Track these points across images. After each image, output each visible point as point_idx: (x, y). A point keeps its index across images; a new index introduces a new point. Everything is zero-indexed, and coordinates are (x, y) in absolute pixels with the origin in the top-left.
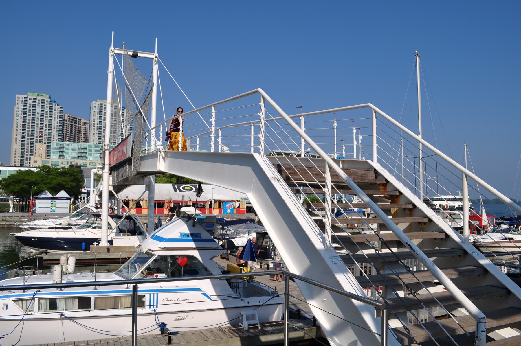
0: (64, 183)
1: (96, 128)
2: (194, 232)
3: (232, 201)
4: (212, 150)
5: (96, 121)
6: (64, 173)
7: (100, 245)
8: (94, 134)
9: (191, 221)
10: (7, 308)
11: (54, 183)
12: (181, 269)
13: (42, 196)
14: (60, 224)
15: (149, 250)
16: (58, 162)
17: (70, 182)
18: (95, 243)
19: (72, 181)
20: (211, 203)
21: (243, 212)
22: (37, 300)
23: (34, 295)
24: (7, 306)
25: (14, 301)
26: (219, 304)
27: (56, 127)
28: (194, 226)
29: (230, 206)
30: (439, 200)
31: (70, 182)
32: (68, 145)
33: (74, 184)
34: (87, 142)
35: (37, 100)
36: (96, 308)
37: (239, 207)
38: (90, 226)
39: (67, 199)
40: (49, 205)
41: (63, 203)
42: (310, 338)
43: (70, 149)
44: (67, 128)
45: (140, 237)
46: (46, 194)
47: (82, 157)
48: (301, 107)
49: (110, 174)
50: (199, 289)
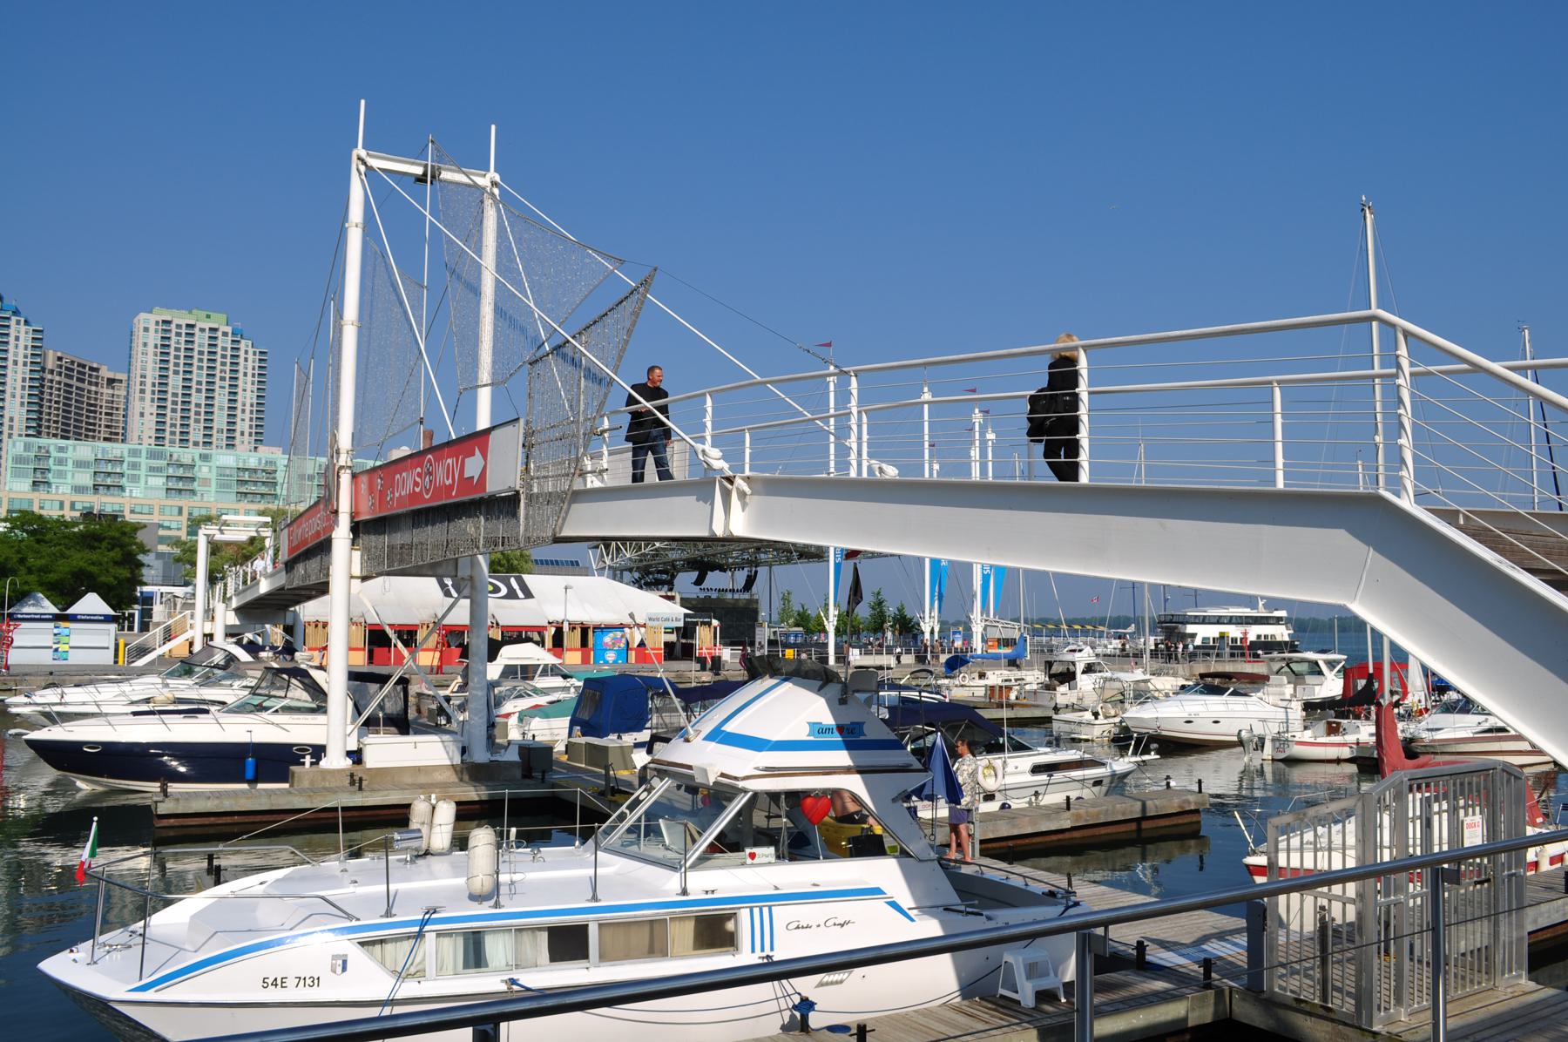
0: (93, 569)
1: (148, 396)
2: (846, 721)
3: (621, 627)
4: (853, 474)
5: (149, 374)
6: (90, 540)
7: (323, 764)
8: (142, 415)
9: (834, 689)
10: (344, 969)
11: (63, 569)
12: (802, 827)
13: (25, 610)
14: (147, 701)
15: (723, 775)
16: (31, 502)
17: (98, 563)
18: (308, 760)
19: (116, 563)
20: (559, 631)
22: (430, 938)
23: (424, 923)
24: (345, 962)
25: (362, 944)
27: (18, 392)
28: (843, 701)
29: (616, 641)
30: (1204, 621)
31: (98, 563)
32: (61, 449)
33: (124, 573)
34: (116, 441)
35: (173, 326)
36: (604, 957)
37: (642, 644)
38: (261, 708)
40: (48, 640)
41: (90, 636)
43: (70, 463)
44: (53, 395)
45: (446, 737)
46: (38, 603)
47: (108, 487)
48: (829, 345)
50: (877, 891)
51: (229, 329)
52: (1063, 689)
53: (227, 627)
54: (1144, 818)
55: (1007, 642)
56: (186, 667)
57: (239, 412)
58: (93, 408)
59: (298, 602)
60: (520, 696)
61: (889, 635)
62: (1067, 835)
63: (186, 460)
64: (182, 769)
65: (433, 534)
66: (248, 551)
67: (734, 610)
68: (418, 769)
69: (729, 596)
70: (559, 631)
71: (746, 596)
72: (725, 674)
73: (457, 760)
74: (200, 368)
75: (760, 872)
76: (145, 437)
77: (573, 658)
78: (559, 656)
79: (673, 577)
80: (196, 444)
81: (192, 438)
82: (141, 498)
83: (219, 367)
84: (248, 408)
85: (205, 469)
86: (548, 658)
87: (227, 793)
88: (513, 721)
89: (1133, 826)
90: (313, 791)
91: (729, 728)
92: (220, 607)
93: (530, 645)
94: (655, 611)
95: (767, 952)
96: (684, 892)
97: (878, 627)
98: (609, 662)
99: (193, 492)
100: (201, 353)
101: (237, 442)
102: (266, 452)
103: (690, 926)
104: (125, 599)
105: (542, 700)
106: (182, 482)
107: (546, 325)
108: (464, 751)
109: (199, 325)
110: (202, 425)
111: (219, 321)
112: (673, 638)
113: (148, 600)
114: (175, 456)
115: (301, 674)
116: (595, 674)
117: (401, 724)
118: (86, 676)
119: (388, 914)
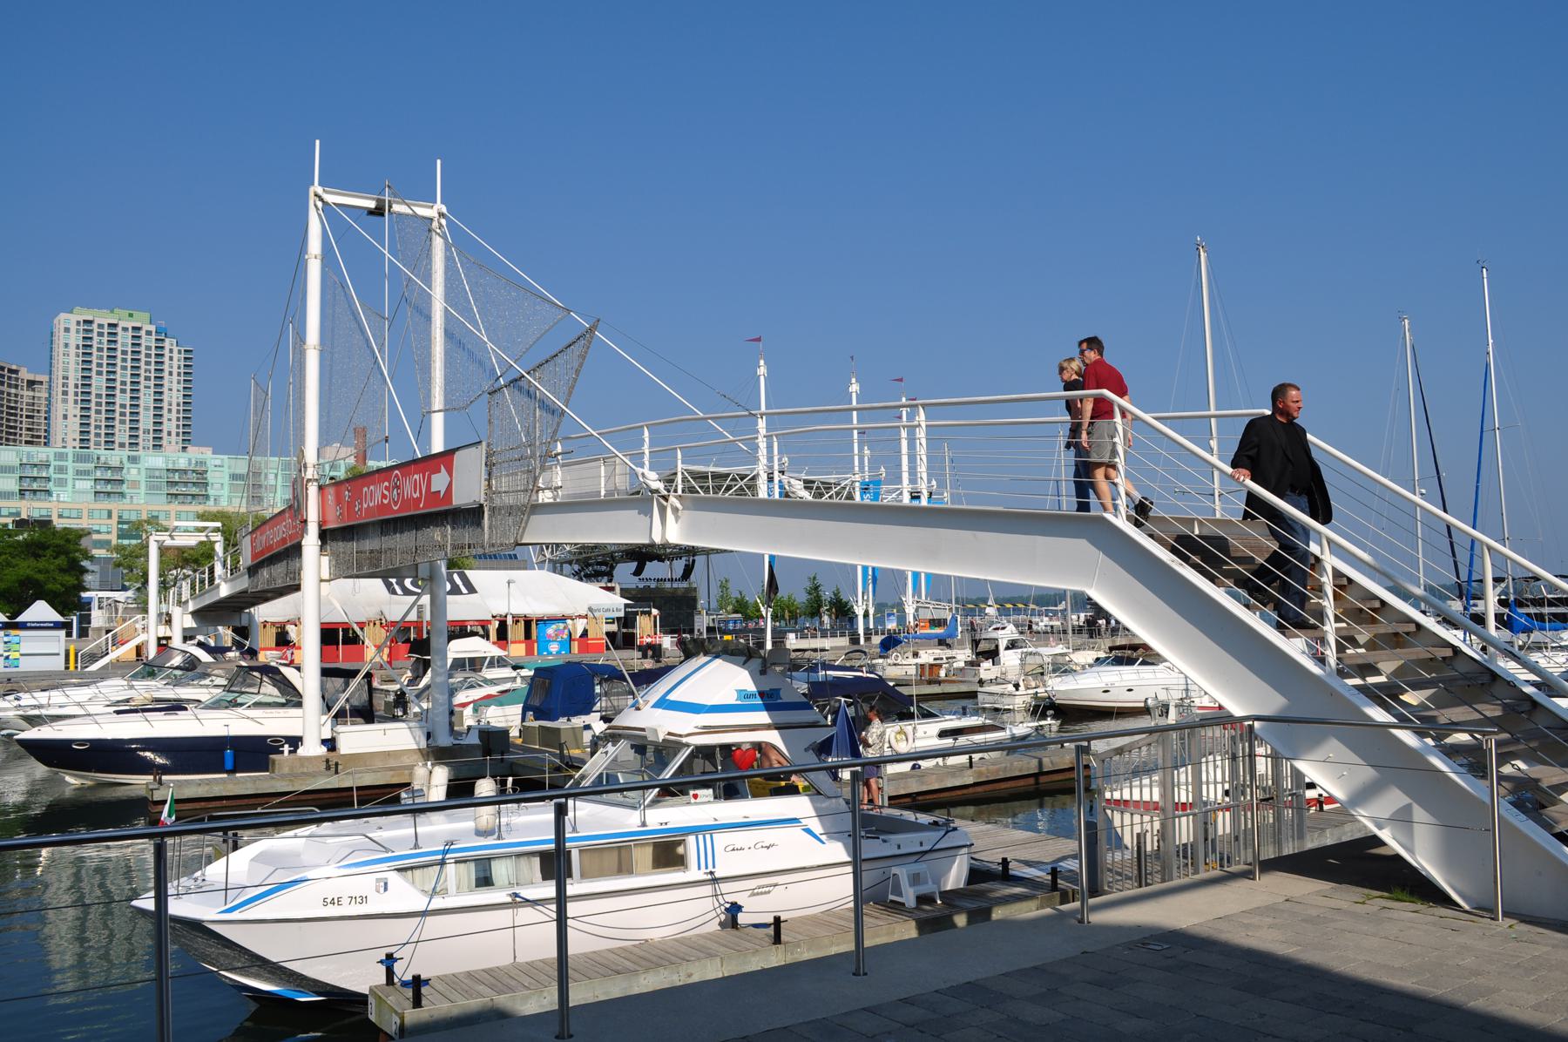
0: (40, 577)
1: (71, 397)
2: (766, 688)
3: (563, 619)
5: (71, 374)
6: (33, 549)
7: (301, 751)
8: (65, 417)
11: (11, 576)
12: (730, 772)
14: (127, 701)
17: (21, 572)
18: (286, 748)
19: (62, 570)
20: (503, 624)
21: (597, 649)
23: (445, 852)
25: (398, 870)
26: (837, 851)
28: (763, 672)
31: (21, 572)
33: (70, 580)
34: (38, 444)
35: (95, 326)
36: (584, 876)
37: (585, 633)
38: (234, 704)
39: (57, 626)
42: (1520, 774)
47: (109, 494)
48: (759, 340)
49: (322, 548)
51: (153, 328)
52: (987, 664)
53: (185, 630)
54: (1041, 773)
55: (935, 623)
56: (150, 670)
57: (165, 412)
58: (13, 411)
59: (253, 604)
60: (471, 687)
61: (826, 619)
62: (971, 790)
63: (114, 462)
64: (159, 760)
65: (403, 541)
66: (197, 558)
67: (671, 605)
68: (388, 754)
69: (668, 585)
70: (503, 624)
71: (685, 585)
72: (665, 661)
73: (423, 744)
74: (124, 368)
75: (701, 809)
76: (69, 439)
77: (517, 650)
78: (504, 648)
79: (612, 568)
80: (122, 445)
81: (117, 439)
82: (70, 503)
83: (143, 366)
84: (174, 408)
85: (134, 471)
86: (496, 652)
87: (209, 782)
88: (468, 711)
89: (1032, 781)
90: (293, 776)
91: (671, 697)
92: (176, 612)
93: (477, 638)
94: (596, 602)
95: (710, 868)
96: (644, 824)
97: (814, 610)
98: (553, 652)
99: (122, 495)
100: (124, 353)
101: (164, 442)
102: (195, 453)
103: (649, 851)
104: (70, 602)
105: (493, 690)
106: (111, 485)
107: (500, 361)
108: (429, 736)
109: (122, 324)
110: (128, 426)
111: (142, 320)
112: (614, 628)
113: (87, 606)
114: (103, 459)
115: (269, 671)
116: (540, 663)
117: (366, 714)
118: (49, 681)
119: (416, 846)
